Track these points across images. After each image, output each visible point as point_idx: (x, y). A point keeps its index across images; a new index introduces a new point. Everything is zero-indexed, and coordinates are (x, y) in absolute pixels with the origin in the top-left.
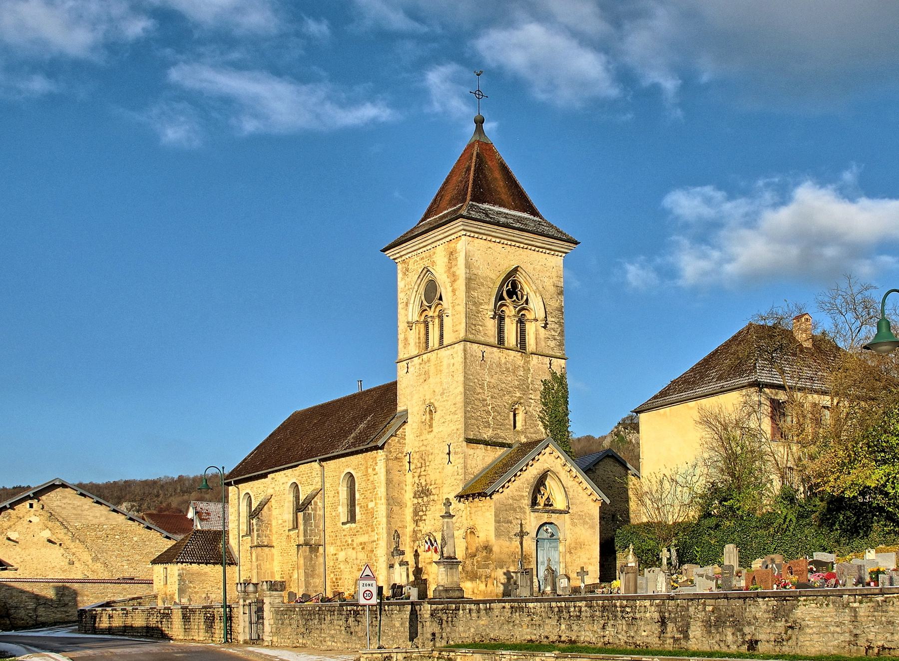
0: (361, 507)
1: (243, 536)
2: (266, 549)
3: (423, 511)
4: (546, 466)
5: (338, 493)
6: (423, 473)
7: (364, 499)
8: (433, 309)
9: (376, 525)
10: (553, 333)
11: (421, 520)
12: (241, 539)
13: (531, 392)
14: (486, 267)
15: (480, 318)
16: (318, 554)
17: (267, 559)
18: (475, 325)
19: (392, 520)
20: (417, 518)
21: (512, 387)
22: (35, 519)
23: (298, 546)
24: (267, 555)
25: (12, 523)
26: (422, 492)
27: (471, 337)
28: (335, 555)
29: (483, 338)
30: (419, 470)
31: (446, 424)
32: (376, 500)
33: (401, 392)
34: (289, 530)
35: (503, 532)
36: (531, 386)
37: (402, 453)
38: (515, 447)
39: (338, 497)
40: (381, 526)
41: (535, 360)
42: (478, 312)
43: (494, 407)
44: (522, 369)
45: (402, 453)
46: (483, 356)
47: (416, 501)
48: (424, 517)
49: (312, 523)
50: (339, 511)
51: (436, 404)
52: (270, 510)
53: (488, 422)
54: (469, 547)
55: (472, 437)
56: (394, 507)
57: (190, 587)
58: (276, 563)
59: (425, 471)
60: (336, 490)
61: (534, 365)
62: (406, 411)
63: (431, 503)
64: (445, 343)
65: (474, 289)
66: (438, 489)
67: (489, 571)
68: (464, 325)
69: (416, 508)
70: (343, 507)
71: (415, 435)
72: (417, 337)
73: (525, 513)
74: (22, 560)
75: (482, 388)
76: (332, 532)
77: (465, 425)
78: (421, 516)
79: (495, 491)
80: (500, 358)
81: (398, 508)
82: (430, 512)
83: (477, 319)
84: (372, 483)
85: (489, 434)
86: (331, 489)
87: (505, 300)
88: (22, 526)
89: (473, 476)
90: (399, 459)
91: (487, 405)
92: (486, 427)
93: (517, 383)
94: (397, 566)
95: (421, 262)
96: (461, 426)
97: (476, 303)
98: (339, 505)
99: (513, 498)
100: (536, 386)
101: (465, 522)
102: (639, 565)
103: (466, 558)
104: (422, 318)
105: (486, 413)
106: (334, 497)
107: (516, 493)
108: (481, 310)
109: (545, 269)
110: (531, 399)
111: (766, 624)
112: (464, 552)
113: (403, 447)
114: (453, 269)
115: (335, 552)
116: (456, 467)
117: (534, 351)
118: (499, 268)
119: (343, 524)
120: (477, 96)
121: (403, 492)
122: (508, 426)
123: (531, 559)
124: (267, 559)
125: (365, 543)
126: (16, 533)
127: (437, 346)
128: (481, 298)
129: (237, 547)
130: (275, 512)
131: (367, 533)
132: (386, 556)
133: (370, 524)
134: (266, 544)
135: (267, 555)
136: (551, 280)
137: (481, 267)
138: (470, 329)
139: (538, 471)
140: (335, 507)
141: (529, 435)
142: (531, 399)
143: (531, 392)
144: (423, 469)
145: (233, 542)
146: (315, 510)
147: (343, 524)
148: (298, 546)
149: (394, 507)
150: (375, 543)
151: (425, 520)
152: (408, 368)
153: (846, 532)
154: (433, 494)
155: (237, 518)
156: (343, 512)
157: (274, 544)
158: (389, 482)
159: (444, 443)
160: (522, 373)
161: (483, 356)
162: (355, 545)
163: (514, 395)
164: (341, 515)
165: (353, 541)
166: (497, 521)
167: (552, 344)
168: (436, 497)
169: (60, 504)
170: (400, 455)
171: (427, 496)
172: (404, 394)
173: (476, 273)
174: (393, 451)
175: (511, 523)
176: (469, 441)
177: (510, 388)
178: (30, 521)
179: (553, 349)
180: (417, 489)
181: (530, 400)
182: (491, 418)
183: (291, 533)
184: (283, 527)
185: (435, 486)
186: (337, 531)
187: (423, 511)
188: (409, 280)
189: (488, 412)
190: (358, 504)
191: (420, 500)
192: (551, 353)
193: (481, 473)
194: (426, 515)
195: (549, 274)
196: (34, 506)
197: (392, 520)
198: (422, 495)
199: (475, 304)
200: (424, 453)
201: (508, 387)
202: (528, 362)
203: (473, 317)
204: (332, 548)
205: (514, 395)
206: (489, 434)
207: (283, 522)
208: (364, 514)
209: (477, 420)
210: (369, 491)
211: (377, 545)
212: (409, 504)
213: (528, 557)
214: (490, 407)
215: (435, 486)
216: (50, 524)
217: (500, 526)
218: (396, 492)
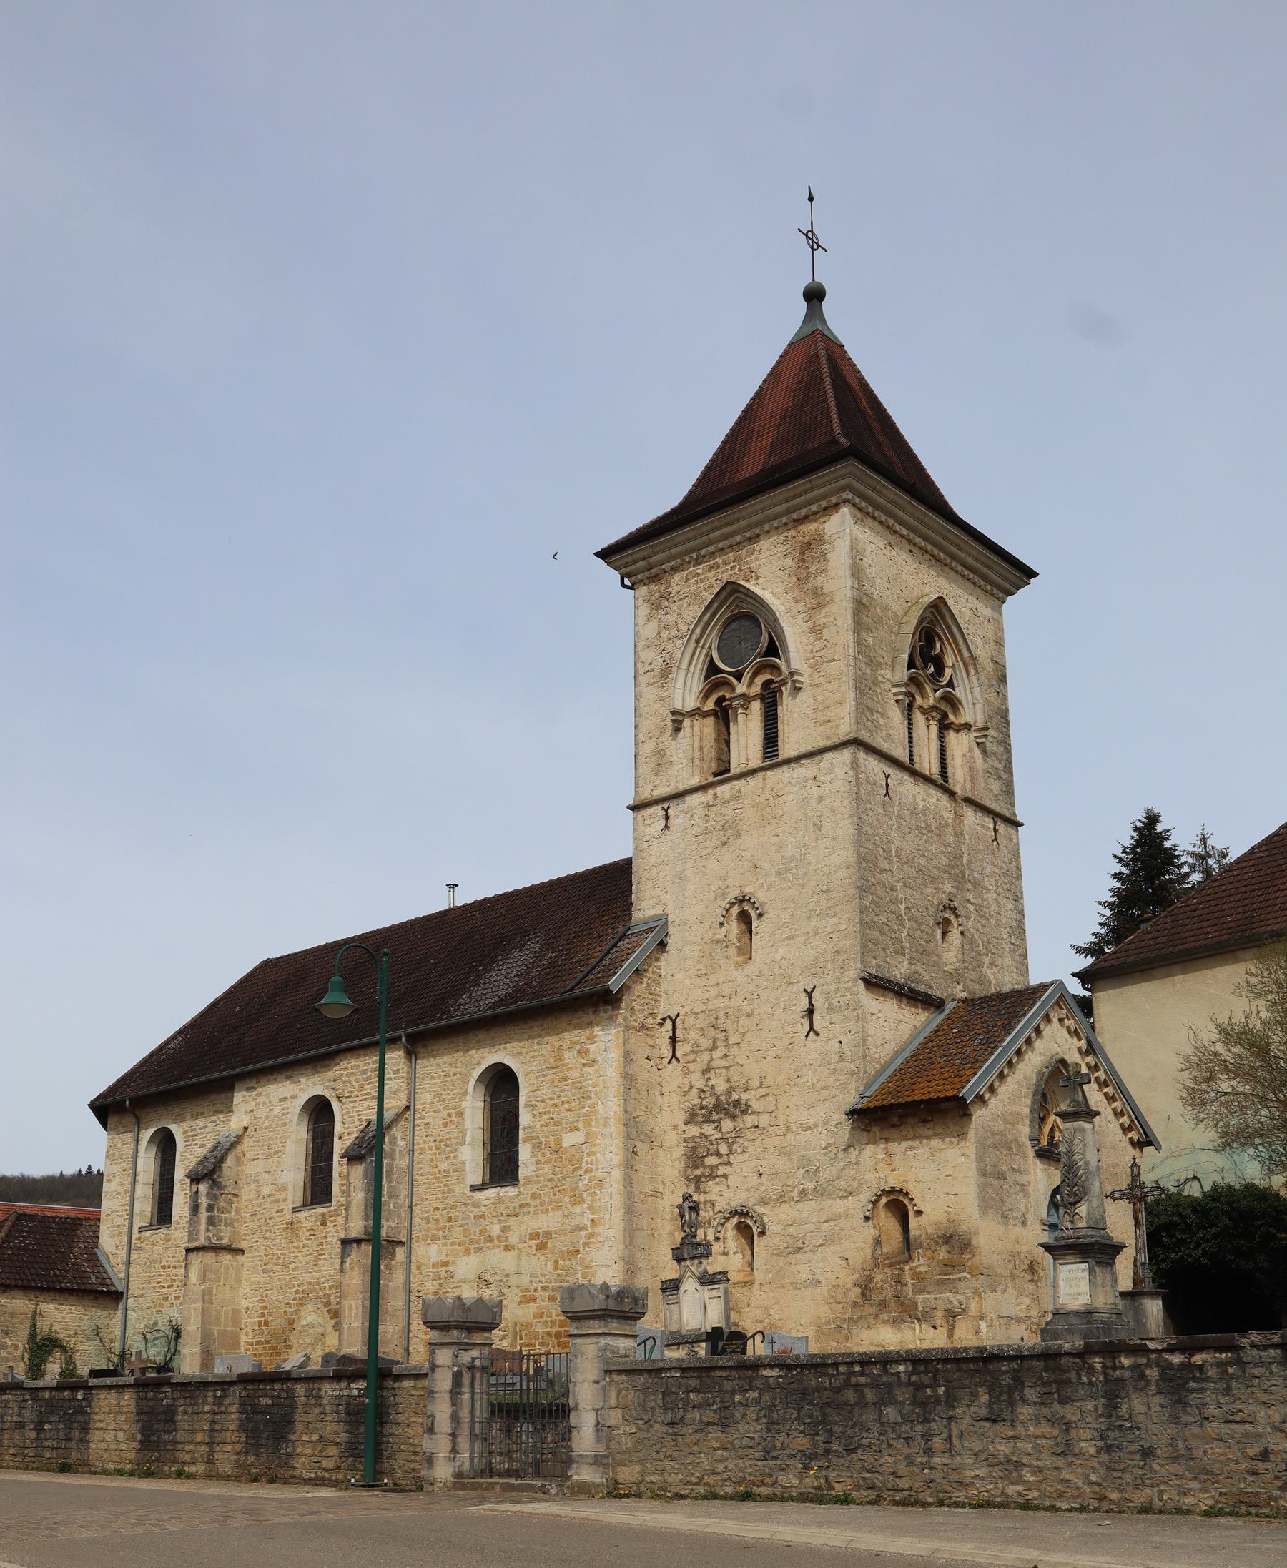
0: (537, 1146)
1: (141, 1230)
2: (227, 1257)
3: (718, 1154)
5: (460, 1114)
6: (718, 1063)
7: (547, 1124)
8: (746, 678)
9: (588, 1188)
11: (712, 1177)
12: (135, 1235)
16: (393, 1263)
17: (226, 1279)
20: (698, 1172)
23: (346, 1242)
24: (227, 1268)
26: (717, 1107)
27: (865, 736)
28: (445, 1264)
30: (705, 1057)
31: (800, 939)
32: (587, 1123)
33: (645, 875)
34: (295, 1210)
35: (993, 1199)
37: (653, 1015)
38: (950, 1006)
39: (461, 1123)
40: (607, 1189)
45: (653, 1015)
46: (887, 785)
47: (694, 1131)
48: (722, 1170)
50: (461, 1158)
51: (761, 896)
52: (238, 1159)
53: (899, 940)
54: (884, 1238)
56: (639, 1144)
58: (246, 1288)
59: (725, 1056)
60: (455, 1107)
62: (663, 919)
63: (748, 1134)
64: (788, 748)
65: (868, 630)
66: (771, 1098)
67: (961, 1297)
68: (849, 706)
69: (693, 1150)
70: (473, 1148)
71: (693, 973)
72: (696, 746)
73: (1026, 1157)
75: (888, 858)
76: (437, 1209)
77: (862, 940)
78: (713, 1167)
80: (914, 796)
82: (745, 1157)
84: (578, 1085)
86: (438, 1106)
89: (878, 1066)
90: (647, 1029)
91: (897, 901)
92: (897, 952)
93: (945, 861)
94: (690, 1285)
95: (710, 575)
96: (851, 943)
98: (463, 1143)
101: (870, 1176)
103: (876, 1266)
104: (710, 705)
105: (897, 919)
106: (445, 1125)
107: (1010, 1108)
111: (937, 1443)
112: (869, 1251)
113: (656, 1001)
114: (813, 582)
115: (444, 1258)
116: (834, 1043)
118: (906, 594)
119: (474, 1188)
121: (656, 1110)
124: (226, 1279)
125: (548, 1234)
127: (756, 760)
129: (123, 1255)
130: (250, 1169)
131: (558, 1207)
132: (620, 1263)
133: (569, 1184)
134: (225, 1241)
135: (227, 1268)
140: (448, 1148)
141: (970, 984)
142: (969, 901)
144: (717, 1054)
145: (109, 1242)
147: (474, 1188)
148: (346, 1242)
149: (639, 1144)
150: (583, 1233)
151: (725, 1176)
152: (667, 818)
154: (754, 1113)
155: (129, 1187)
156: (472, 1158)
157: (243, 1244)
158: (629, 1082)
159: (794, 988)
162: (513, 1240)
164: (468, 1167)
165: (506, 1229)
166: (983, 1173)
168: (764, 1120)
171: (733, 1117)
172: (655, 881)
173: (869, 592)
174: (637, 1007)
176: (874, 983)
177: (935, 871)
180: (697, 1102)
181: (969, 906)
183: (301, 1215)
184: (278, 1201)
185: (762, 1091)
186: (453, 1207)
187: (718, 1154)
188: (670, 618)
190: (527, 1140)
191: (709, 1129)
193: (892, 1060)
194: (729, 1163)
198: (715, 1116)
199: (870, 662)
200: (721, 1014)
204: (434, 1249)
206: (903, 970)
207: (278, 1190)
208: (547, 1162)
209: (881, 932)
210: (567, 1106)
211: (591, 1235)
212: (672, 1138)
214: (903, 907)
215: (762, 1091)
218: (643, 1108)
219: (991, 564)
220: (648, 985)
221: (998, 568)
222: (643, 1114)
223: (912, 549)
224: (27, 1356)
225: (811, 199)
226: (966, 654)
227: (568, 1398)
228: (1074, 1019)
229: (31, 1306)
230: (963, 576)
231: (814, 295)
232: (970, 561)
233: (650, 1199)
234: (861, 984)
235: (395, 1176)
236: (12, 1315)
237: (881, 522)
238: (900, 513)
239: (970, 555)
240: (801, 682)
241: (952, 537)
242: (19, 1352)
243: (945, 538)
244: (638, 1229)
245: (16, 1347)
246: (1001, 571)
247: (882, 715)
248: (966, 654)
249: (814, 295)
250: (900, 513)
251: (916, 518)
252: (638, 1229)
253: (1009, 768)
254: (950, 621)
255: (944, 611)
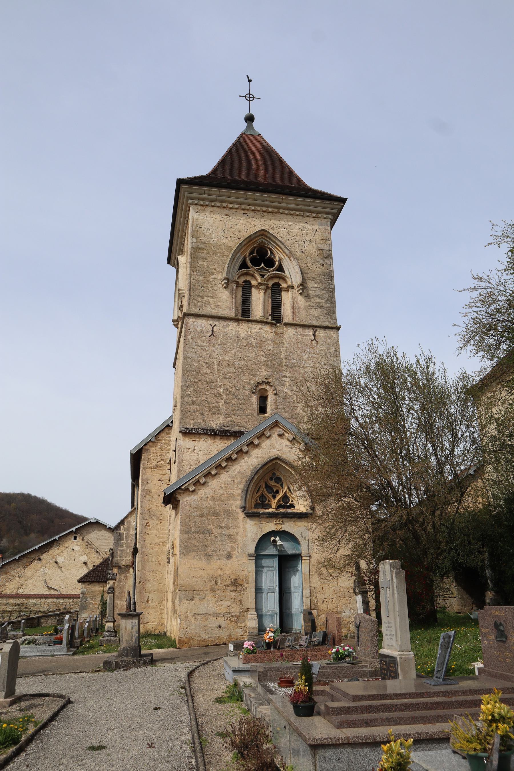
4: (274, 453)
10: (319, 300)
13: (285, 368)
14: (220, 234)
15: (210, 289)
16: (128, 575)
18: (202, 297)
19: (146, 536)
21: (255, 364)
22: (77, 548)
25: (61, 551)
29: (213, 311)
35: (196, 546)
36: (284, 361)
41: (290, 332)
42: (208, 282)
43: (227, 389)
44: (271, 343)
46: (213, 331)
49: (123, 543)
55: (192, 426)
57: (91, 604)
61: (289, 337)
74: (65, 578)
79: (180, 488)
80: (237, 331)
81: (156, 522)
83: (205, 290)
85: (218, 422)
87: (248, 268)
88: (67, 552)
90: (160, 467)
92: (213, 413)
93: (263, 359)
97: (205, 273)
99: (214, 499)
100: (293, 361)
102: (235, 616)
108: (211, 280)
109: (305, 233)
110: (286, 377)
117: (291, 321)
120: (248, 99)
122: (249, 411)
123: (246, 585)
126: (63, 558)
128: (213, 267)
136: (314, 244)
137: (213, 235)
138: (195, 301)
139: (260, 459)
142: (286, 377)
143: (285, 368)
146: (128, 529)
153: (447, 589)
160: (271, 347)
161: (213, 331)
163: (258, 373)
167: (316, 312)
169: (96, 536)
170: (162, 462)
175: (210, 533)
177: (253, 366)
178: (73, 549)
179: (317, 318)
181: (285, 379)
182: (223, 402)
189: (218, 396)
192: (315, 323)
195: (311, 238)
196: (77, 538)
197: (146, 536)
201: (249, 365)
202: (281, 335)
203: (200, 288)
205: (258, 373)
206: (218, 422)
213: (240, 582)
214: (221, 390)
216: (87, 551)
217: (189, 539)
219: (308, 204)
220: (161, 447)
221: (314, 204)
222: (155, 507)
223: (245, 212)
224: (100, 607)
225: (250, 81)
226: (287, 252)
227: (496, 603)
228: (291, 433)
229: (102, 588)
230: (292, 215)
231: (250, 119)
232: (291, 206)
233: (158, 547)
234: (181, 435)
235: (130, 538)
236: (94, 592)
237: (218, 207)
238: (228, 199)
239: (290, 204)
240: (184, 293)
241: (271, 199)
242: (97, 606)
243: (267, 201)
244: (148, 562)
245: (96, 604)
246: (318, 205)
247: (212, 297)
248: (287, 252)
249: (250, 119)
250: (228, 199)
251: (241, 198)
252: (148, 562)
253: (332, 300)
254: (274, 239)
255: (269, 235)
